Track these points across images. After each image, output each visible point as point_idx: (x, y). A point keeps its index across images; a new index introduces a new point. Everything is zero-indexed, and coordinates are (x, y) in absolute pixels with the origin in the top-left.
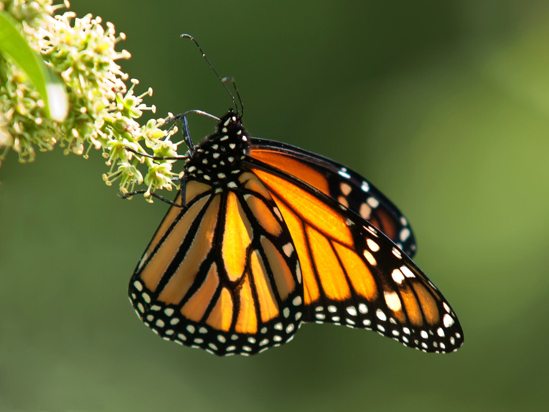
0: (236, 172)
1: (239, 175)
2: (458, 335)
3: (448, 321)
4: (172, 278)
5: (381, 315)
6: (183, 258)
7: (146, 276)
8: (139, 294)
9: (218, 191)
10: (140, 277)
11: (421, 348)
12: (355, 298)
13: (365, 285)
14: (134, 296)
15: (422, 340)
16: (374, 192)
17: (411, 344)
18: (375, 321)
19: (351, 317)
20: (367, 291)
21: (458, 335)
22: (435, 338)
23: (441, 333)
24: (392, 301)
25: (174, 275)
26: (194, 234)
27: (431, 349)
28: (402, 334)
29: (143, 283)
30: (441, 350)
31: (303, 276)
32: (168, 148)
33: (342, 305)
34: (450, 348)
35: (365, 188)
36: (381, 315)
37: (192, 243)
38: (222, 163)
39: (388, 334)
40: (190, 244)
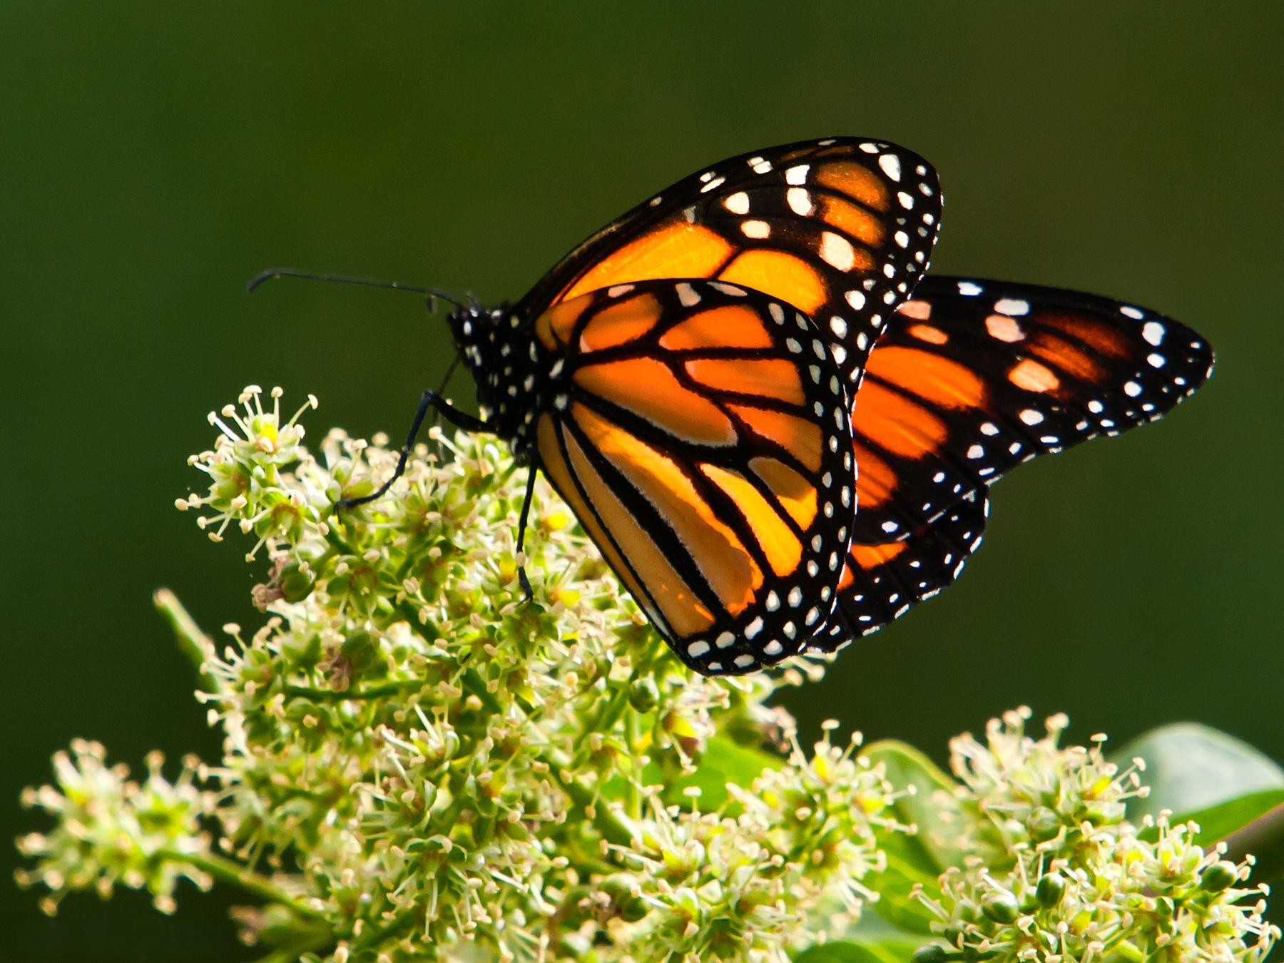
0: (533, 349)
1: (541, 348)
2: (1196, 345)
3: (1153, 333)
4: (700, 568)
5: (1031, 417)
6: (653, 508)
7: (684, 627)
8: (715, 654)
9: (561, 402)
10: (821, 426)
11: (1147, 415)
12: (960, 424)
13: (959, 387)
14: (714, 666)
15: (1136, 403)
16: (781, 158)
17: (1123, 425)
18: (1030, 437)
19: (982, 463)
20: (970, 395)
21: (1196, 345)
22: (1151, 380)
23: (1156, 361)
24: (1031, 377)
25: (697, 562)
26: (630, 486)
27: (1164, 404)
28: (1094, 419)
29: (696, 637)
30: (1182, 390)
31: (669, 619)
32: (1206, 854)
33: (949, 455)
34: (1195, 377)
35: (761, 166)
36: (1031, 417)
37: (648, 498)
38: (508, 371)
39: (1070, 438)
40: (648, 503)
